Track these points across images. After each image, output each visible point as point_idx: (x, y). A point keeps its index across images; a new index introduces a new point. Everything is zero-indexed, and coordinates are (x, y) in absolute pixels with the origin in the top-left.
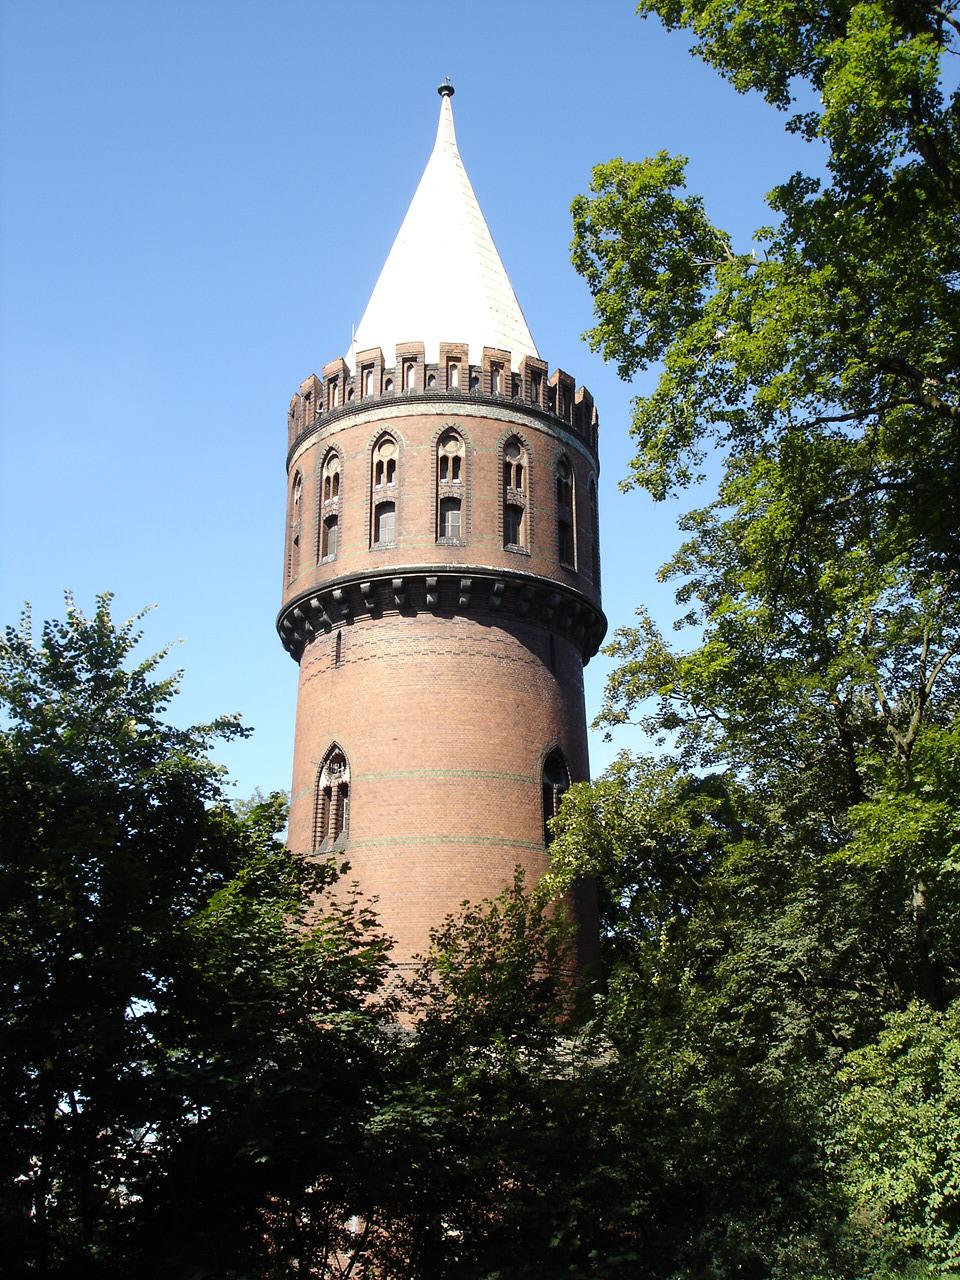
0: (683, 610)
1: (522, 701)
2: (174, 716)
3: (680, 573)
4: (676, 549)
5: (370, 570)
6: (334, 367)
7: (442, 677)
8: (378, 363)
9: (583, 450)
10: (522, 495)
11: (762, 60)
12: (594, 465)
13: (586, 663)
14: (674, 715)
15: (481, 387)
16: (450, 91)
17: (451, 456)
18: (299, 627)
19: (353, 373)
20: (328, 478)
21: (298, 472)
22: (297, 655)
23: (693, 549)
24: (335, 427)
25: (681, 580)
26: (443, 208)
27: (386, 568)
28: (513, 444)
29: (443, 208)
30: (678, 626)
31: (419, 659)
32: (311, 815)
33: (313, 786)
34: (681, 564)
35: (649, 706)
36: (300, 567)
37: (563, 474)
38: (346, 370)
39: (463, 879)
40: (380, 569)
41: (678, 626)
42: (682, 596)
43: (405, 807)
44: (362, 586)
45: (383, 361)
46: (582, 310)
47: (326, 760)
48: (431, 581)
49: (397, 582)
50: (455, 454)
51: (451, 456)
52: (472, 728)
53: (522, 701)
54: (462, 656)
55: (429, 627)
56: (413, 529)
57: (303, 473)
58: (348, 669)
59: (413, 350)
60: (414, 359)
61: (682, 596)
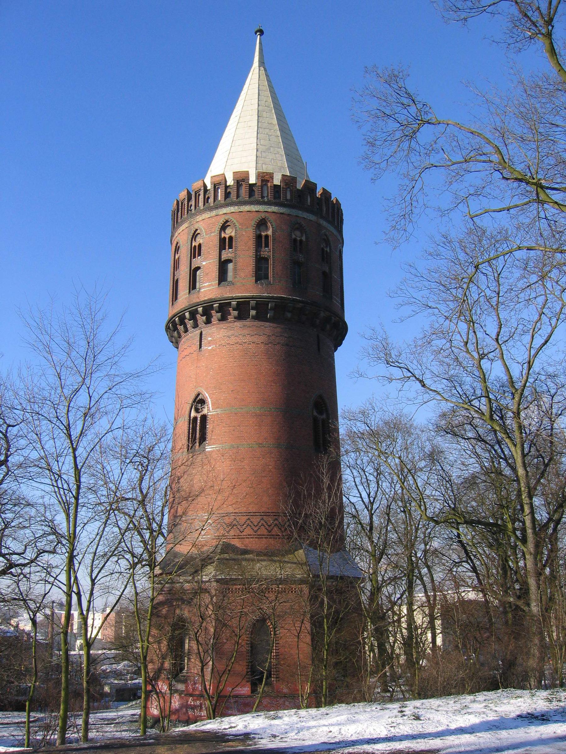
6: (197, 185)
8: (223, 182)
9: (335, 232)
10: (265, 252)
12: (341, 241)
13: (336, 350)
15: (257, 196)
16: (261, 32)
18: (176, 327)
19: (209, 187)
20: (195, 246)
21: (177, 243)
22: (176, 344)
28: (262, 224)
31: (411, 417)
32: (186, 431)
33: (187, 418)
37: (325, 245)
38: (205, 186)
39: (270, 467)
44: (215, 305)
45: (226, 181)
47: (194, 401)
48: (253, 303)
49: (234, 303)
54: (270, 345)
56: (242, 275)
57: (181, 244)
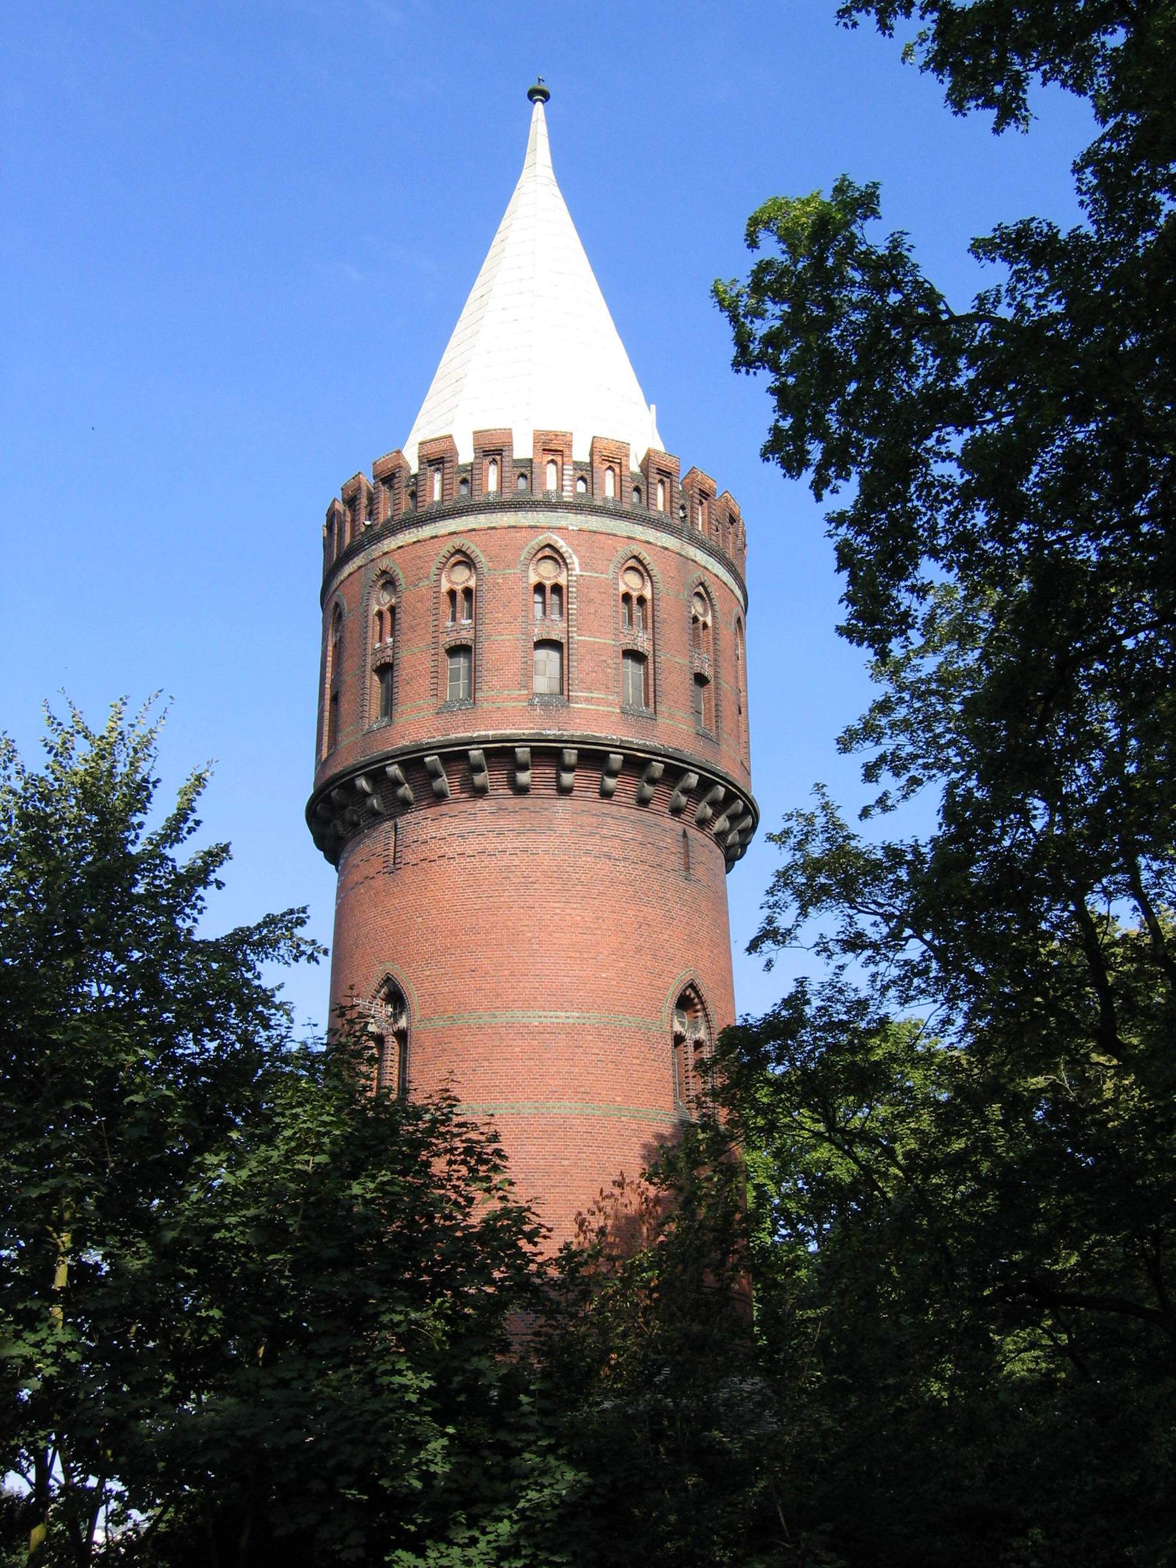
0: (872, 793)
1: (645, 918)
2: (214, 919)
3: (868, 744)
4: (864, 709)
5: (439, 738)
7: (536, 886)
11: (977, 67)
14: (860, 935)
17: (459, 588)
21: (337, 605)
23: (884, 707)
24: (390, 544)
25: (869, 752)
26: (537, 247)
27: (459, 735)
29: (537, 247)
30: (865, 813)
34: (869, 731)
35: (828, 921)
36: (341, 734)
39: (566, 1162)
40: (453, 736)
41: (865, 813)
42: (870, 773)
43: (485, 1063)
46: (754, 404)
50: (553, 582)
51: (459, 588)
52: (578, 955)
53: (645, 918)
55: (519, 818)
58: (407, 875)
59: (498, 442)
60: (499, 452)
61: (870, 773)
